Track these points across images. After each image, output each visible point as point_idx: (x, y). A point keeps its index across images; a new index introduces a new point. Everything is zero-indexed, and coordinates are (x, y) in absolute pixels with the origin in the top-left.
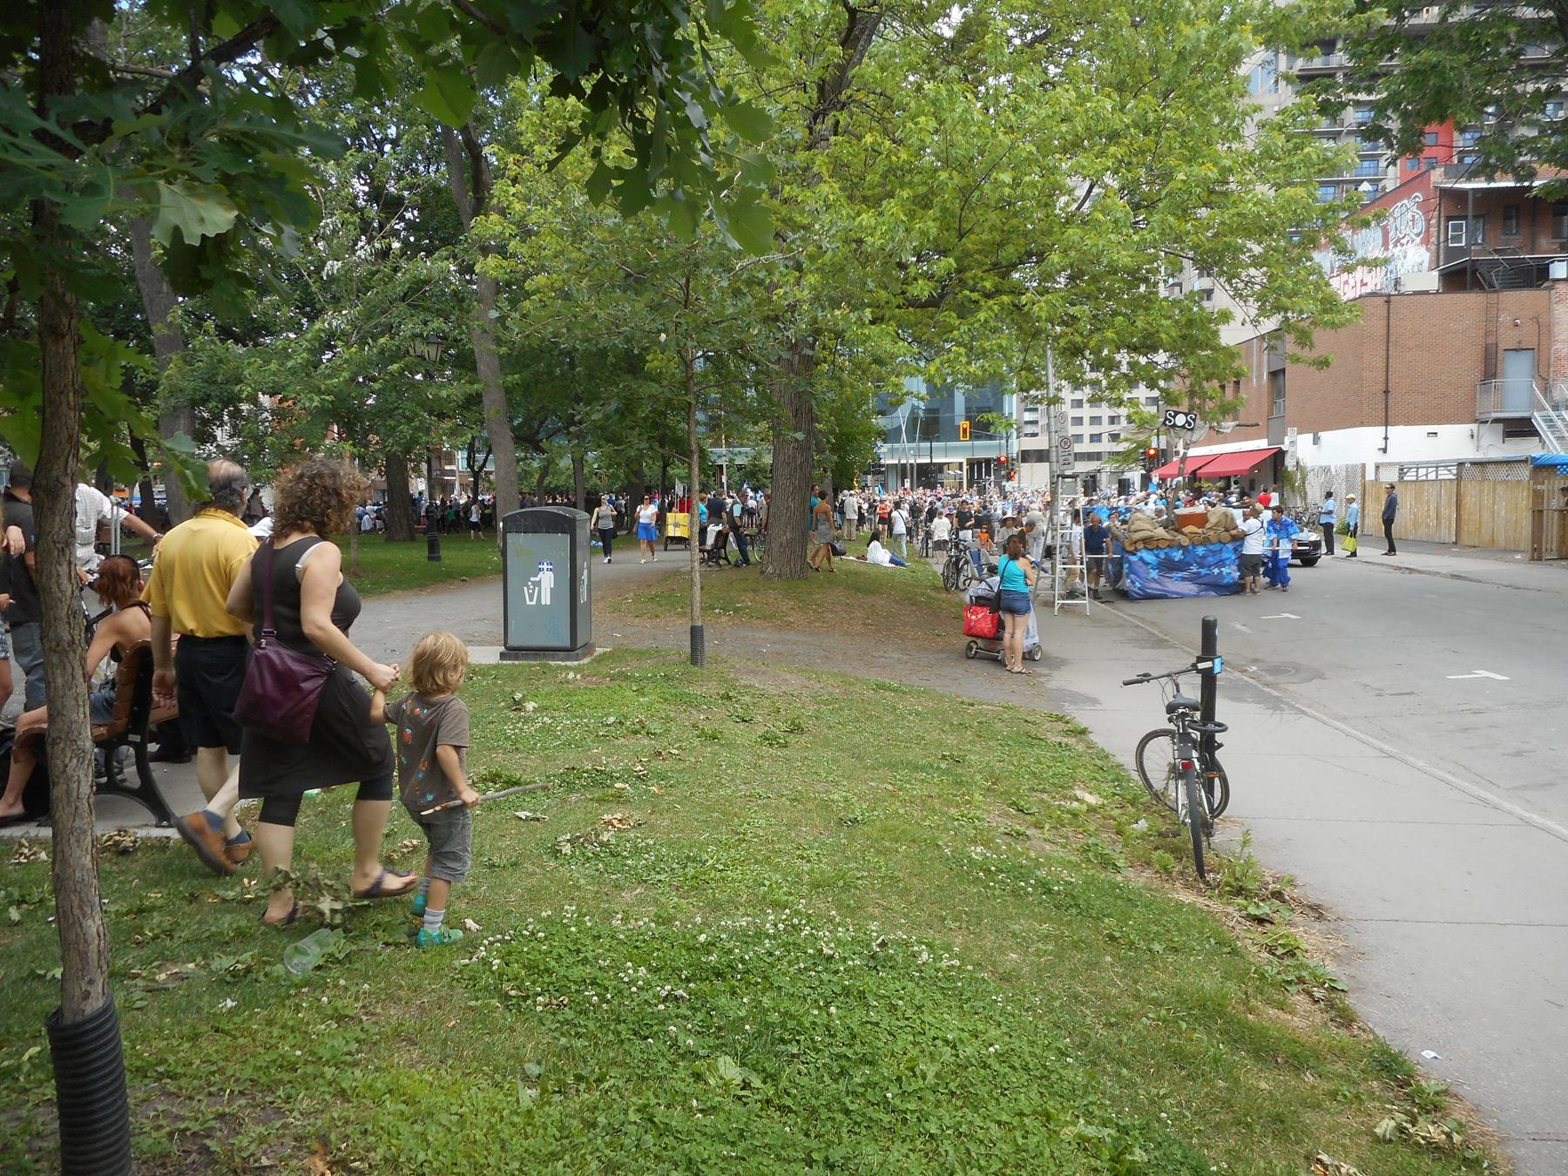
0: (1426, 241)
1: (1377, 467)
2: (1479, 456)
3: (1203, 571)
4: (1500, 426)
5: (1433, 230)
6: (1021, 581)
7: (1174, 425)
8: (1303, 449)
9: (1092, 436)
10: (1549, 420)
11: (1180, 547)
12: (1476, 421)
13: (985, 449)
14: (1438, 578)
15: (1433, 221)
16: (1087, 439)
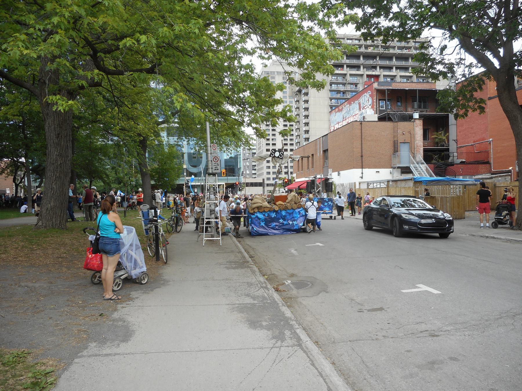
0: (372, 107)
1: (360, 183)
2: (395, 178)
3: (285, 222)
4: (400, 170)
5: (375, 103)
6: (112, 229)
7: (275, 156)
8: (335, 178)
10: (415, 168)
11: (274, 211)
12: (392, 168)
13: (232, 180)
14: (358, 220)
15: (375, 100)
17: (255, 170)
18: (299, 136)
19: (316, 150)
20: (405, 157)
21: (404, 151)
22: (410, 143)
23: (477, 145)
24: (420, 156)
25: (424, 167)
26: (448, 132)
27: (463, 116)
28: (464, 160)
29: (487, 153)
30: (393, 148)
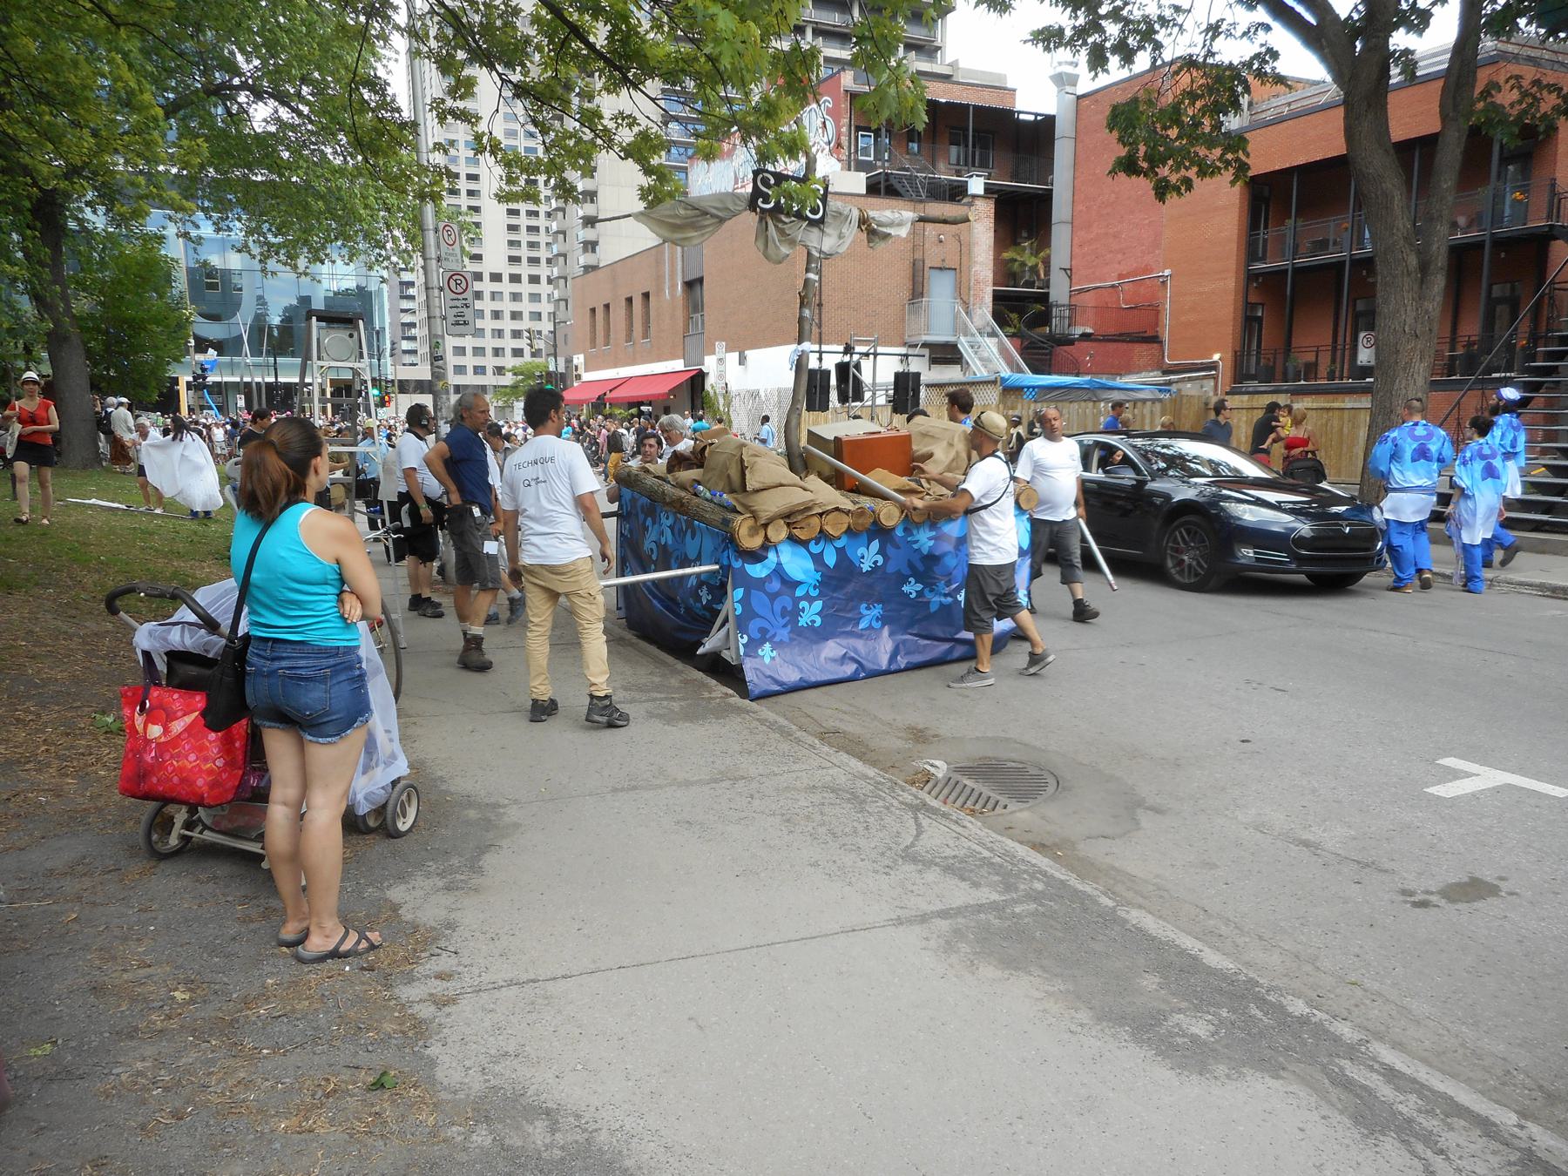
5: (844, 140)
9: (493, 293)
15: (844, 129)
16: (470, 370)
17: (414, 338)
18: (564, 233)
19: (659, 278)
20: (941, 316)
21: (940, 291)
22: (957, 269)
23: (1126, 287)
24: (984, 311)
25: (990, 346)
26: (1048, 245)
27: (1178, 190)
28: (1089, 330)
29: (1155, 310)
30: (909, 285)
